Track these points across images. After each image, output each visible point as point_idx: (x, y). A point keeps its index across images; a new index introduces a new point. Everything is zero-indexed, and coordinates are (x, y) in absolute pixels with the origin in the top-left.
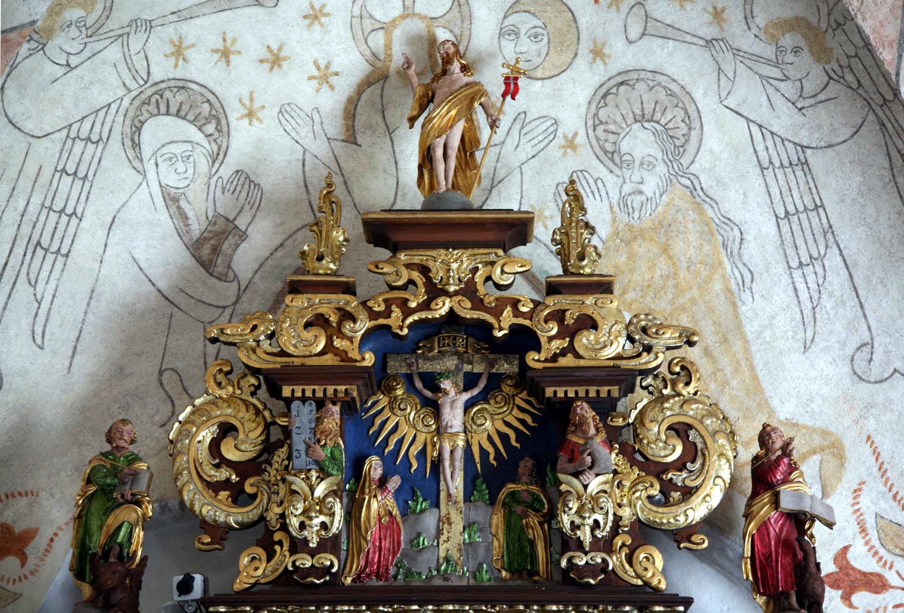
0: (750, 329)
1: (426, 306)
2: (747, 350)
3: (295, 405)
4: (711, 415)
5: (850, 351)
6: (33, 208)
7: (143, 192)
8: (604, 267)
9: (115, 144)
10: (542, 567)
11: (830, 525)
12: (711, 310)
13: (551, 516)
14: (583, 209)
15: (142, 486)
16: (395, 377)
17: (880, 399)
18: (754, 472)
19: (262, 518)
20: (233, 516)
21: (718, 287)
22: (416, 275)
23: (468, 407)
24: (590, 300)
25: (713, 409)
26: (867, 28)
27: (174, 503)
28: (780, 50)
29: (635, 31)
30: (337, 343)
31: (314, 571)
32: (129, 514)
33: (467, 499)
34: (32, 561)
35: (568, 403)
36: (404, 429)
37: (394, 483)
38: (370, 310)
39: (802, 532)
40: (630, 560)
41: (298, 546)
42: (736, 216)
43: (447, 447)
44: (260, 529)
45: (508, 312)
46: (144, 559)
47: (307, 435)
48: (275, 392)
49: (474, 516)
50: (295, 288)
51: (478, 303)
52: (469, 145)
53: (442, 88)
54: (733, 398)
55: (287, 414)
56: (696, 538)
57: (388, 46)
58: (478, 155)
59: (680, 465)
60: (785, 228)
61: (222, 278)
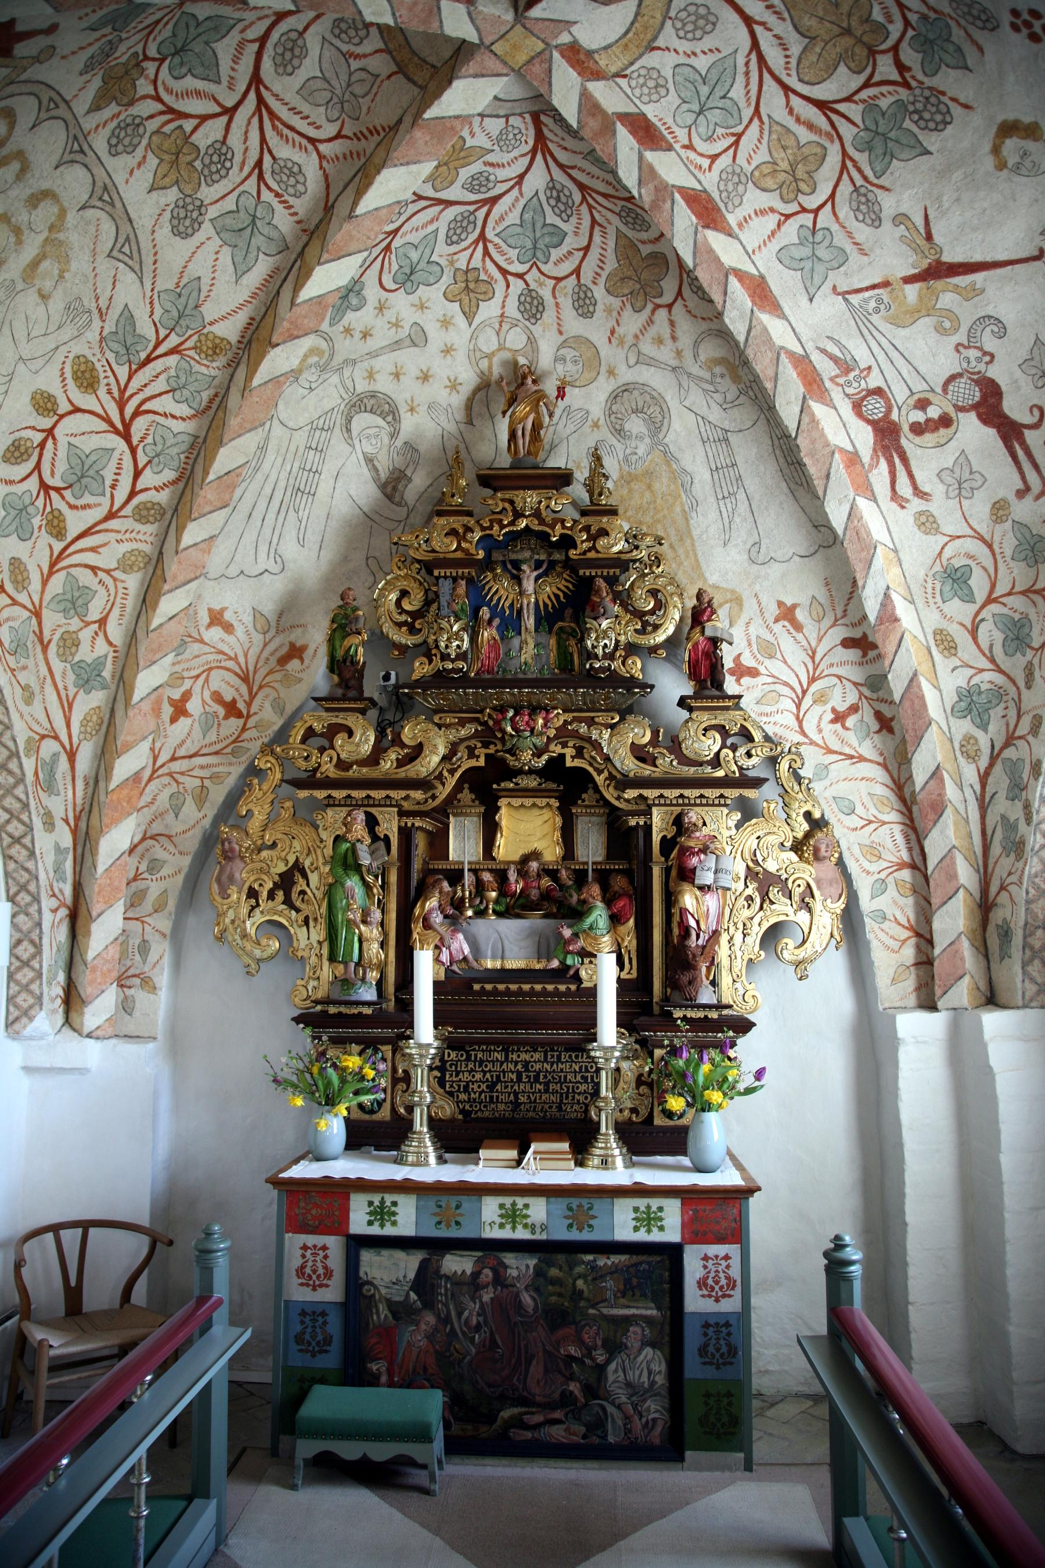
0: (695, 533)
1: (512, 523)
2: (693, 545)
3: (441, 581)
4: (670, 584)
5: (748, 546)
6: (295, 470)
7: (353, 458)
8: (612, 501)
9: (337, 430)
10: (576, 667)
11: (731, 644)
12: (674, 522)
13: (582, 640)
14: (602, 466)
15: (361, 625)
16: (496, 562)
17: (763, 574)
18: (693, 615)
19: (425, 642)
20: (410, 641)
21: (678, 509)
22: (507, 505)
23: (537, 579)
24: (605, 519)
25: (672, 581)
26: (758, 368)
27: (377, 631)
28: (713, 375)
29: (632, 361)
30: (463, 545)
31: (454, 670)
32: (356, 640)
33: (536, 630)
34: (306, 662)
35: (592, 579)
36: (502, 592)
37: (496, 622)
38: (481, 526)
39: (716, 647)
40: (623, 663)
41: (445, 657)
42: (689, 469)
43: (525, 602)
44: (423, 649)
45: (558, 527)
46: (364, 663)
47: (448, 597)
48: (430, 572)
49: (540, 640)
50: (440, 514)
51: (542, 522)
52: (537, 427)
53: (521, 394)
54: (685, 572)
55: (437, 585)
56: (660, 652)
57: (490, 367)
58: (542, 432)
59: (652, 612)
60: (716, 477)
61: (399, 504)
